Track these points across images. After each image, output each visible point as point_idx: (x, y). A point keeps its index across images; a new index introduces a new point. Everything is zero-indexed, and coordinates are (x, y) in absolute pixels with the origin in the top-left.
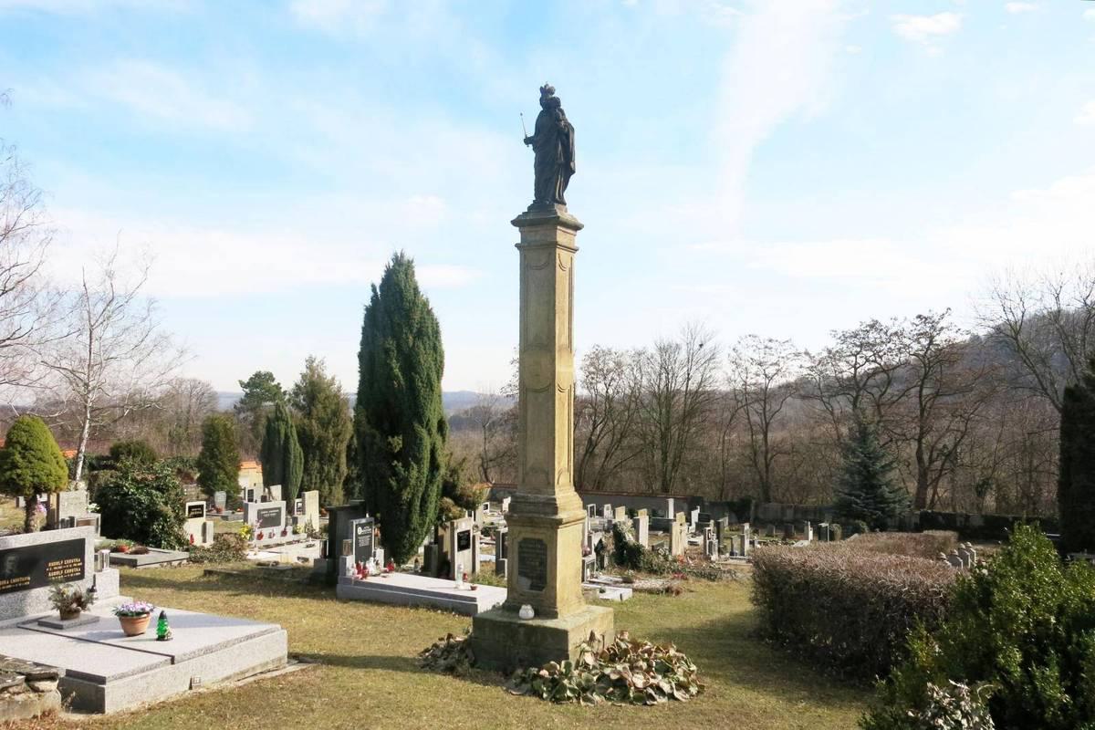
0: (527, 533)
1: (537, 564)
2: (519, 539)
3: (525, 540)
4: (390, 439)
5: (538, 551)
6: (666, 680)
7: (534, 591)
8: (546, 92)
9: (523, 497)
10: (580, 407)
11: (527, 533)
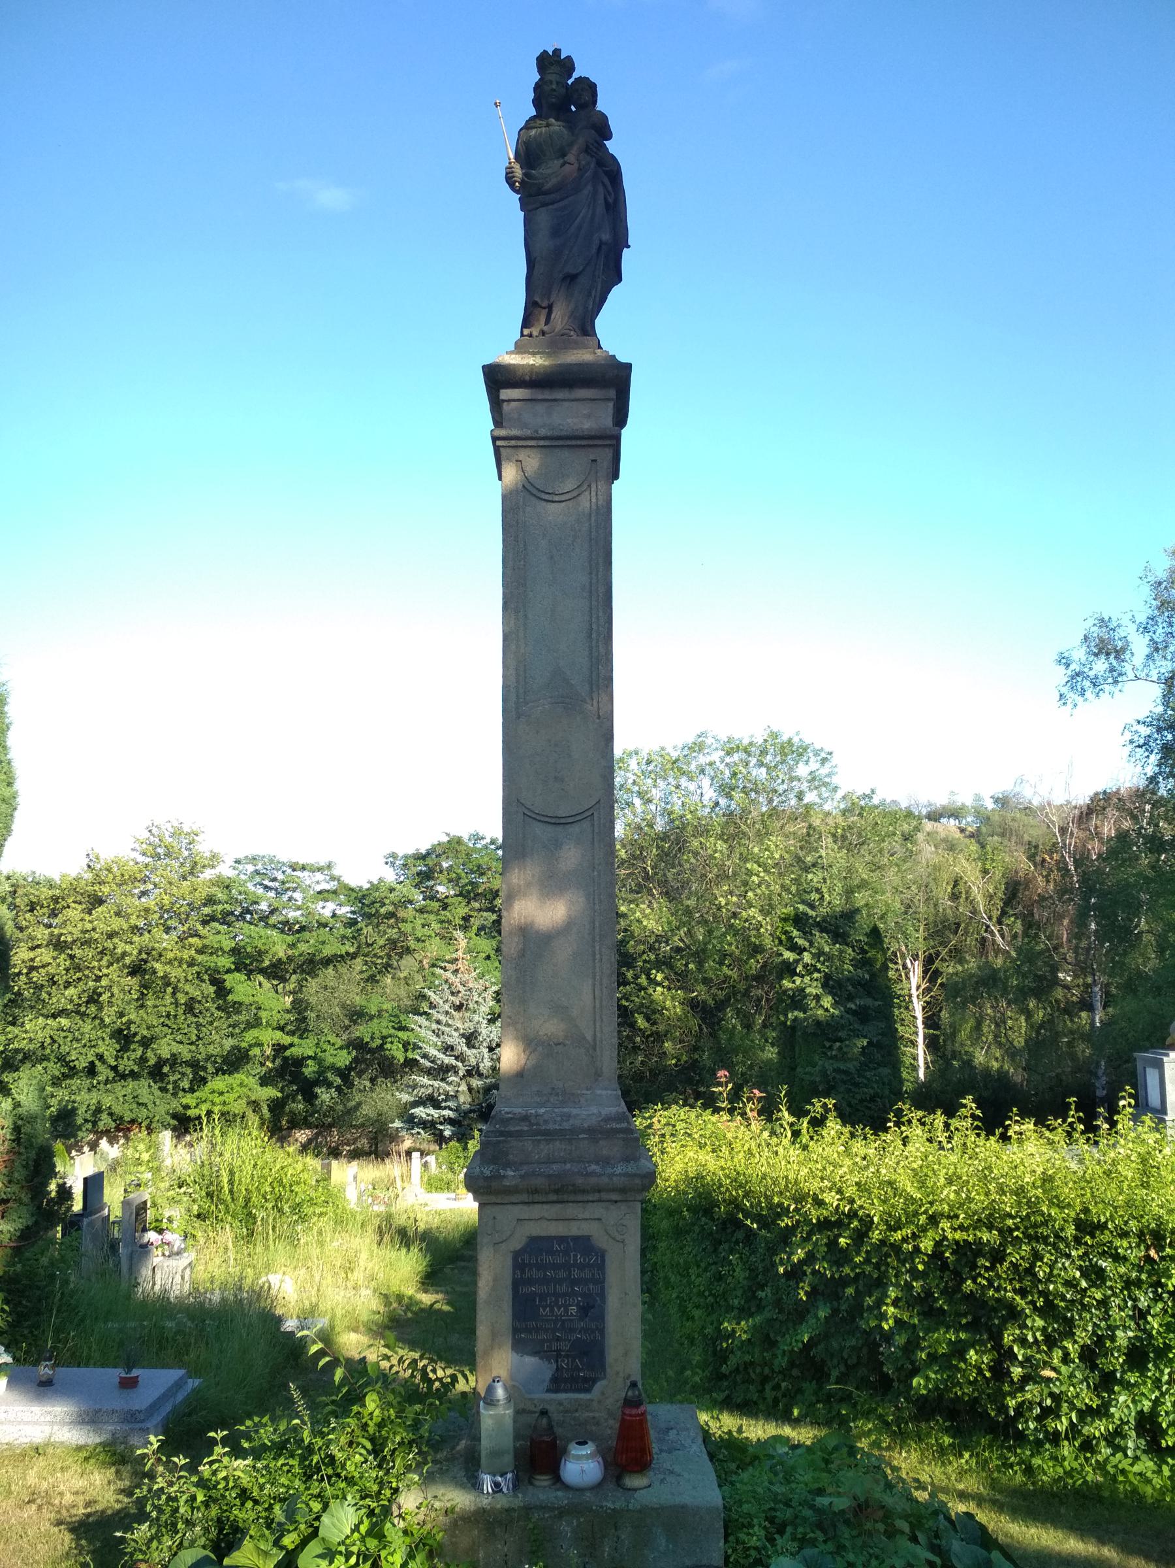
0: (544, 1221)
1: (573, 1310)
2: (517, 1243)
3: (536, 1245)
4: (433, 1192)
5: (576, 1274)
6: (439, 1062)
7: (562, 1396)
8: (553, 65)
9: (525, 1118)
10: (519, 348)
11: (544, 1221)
